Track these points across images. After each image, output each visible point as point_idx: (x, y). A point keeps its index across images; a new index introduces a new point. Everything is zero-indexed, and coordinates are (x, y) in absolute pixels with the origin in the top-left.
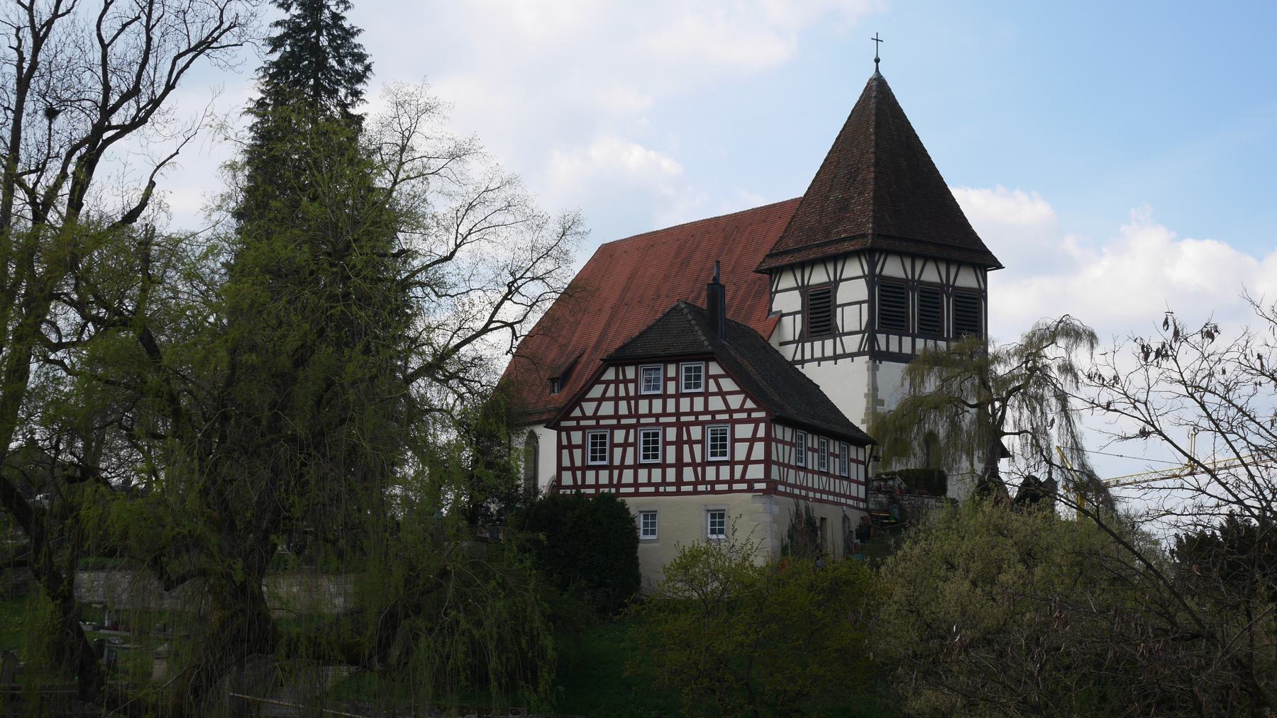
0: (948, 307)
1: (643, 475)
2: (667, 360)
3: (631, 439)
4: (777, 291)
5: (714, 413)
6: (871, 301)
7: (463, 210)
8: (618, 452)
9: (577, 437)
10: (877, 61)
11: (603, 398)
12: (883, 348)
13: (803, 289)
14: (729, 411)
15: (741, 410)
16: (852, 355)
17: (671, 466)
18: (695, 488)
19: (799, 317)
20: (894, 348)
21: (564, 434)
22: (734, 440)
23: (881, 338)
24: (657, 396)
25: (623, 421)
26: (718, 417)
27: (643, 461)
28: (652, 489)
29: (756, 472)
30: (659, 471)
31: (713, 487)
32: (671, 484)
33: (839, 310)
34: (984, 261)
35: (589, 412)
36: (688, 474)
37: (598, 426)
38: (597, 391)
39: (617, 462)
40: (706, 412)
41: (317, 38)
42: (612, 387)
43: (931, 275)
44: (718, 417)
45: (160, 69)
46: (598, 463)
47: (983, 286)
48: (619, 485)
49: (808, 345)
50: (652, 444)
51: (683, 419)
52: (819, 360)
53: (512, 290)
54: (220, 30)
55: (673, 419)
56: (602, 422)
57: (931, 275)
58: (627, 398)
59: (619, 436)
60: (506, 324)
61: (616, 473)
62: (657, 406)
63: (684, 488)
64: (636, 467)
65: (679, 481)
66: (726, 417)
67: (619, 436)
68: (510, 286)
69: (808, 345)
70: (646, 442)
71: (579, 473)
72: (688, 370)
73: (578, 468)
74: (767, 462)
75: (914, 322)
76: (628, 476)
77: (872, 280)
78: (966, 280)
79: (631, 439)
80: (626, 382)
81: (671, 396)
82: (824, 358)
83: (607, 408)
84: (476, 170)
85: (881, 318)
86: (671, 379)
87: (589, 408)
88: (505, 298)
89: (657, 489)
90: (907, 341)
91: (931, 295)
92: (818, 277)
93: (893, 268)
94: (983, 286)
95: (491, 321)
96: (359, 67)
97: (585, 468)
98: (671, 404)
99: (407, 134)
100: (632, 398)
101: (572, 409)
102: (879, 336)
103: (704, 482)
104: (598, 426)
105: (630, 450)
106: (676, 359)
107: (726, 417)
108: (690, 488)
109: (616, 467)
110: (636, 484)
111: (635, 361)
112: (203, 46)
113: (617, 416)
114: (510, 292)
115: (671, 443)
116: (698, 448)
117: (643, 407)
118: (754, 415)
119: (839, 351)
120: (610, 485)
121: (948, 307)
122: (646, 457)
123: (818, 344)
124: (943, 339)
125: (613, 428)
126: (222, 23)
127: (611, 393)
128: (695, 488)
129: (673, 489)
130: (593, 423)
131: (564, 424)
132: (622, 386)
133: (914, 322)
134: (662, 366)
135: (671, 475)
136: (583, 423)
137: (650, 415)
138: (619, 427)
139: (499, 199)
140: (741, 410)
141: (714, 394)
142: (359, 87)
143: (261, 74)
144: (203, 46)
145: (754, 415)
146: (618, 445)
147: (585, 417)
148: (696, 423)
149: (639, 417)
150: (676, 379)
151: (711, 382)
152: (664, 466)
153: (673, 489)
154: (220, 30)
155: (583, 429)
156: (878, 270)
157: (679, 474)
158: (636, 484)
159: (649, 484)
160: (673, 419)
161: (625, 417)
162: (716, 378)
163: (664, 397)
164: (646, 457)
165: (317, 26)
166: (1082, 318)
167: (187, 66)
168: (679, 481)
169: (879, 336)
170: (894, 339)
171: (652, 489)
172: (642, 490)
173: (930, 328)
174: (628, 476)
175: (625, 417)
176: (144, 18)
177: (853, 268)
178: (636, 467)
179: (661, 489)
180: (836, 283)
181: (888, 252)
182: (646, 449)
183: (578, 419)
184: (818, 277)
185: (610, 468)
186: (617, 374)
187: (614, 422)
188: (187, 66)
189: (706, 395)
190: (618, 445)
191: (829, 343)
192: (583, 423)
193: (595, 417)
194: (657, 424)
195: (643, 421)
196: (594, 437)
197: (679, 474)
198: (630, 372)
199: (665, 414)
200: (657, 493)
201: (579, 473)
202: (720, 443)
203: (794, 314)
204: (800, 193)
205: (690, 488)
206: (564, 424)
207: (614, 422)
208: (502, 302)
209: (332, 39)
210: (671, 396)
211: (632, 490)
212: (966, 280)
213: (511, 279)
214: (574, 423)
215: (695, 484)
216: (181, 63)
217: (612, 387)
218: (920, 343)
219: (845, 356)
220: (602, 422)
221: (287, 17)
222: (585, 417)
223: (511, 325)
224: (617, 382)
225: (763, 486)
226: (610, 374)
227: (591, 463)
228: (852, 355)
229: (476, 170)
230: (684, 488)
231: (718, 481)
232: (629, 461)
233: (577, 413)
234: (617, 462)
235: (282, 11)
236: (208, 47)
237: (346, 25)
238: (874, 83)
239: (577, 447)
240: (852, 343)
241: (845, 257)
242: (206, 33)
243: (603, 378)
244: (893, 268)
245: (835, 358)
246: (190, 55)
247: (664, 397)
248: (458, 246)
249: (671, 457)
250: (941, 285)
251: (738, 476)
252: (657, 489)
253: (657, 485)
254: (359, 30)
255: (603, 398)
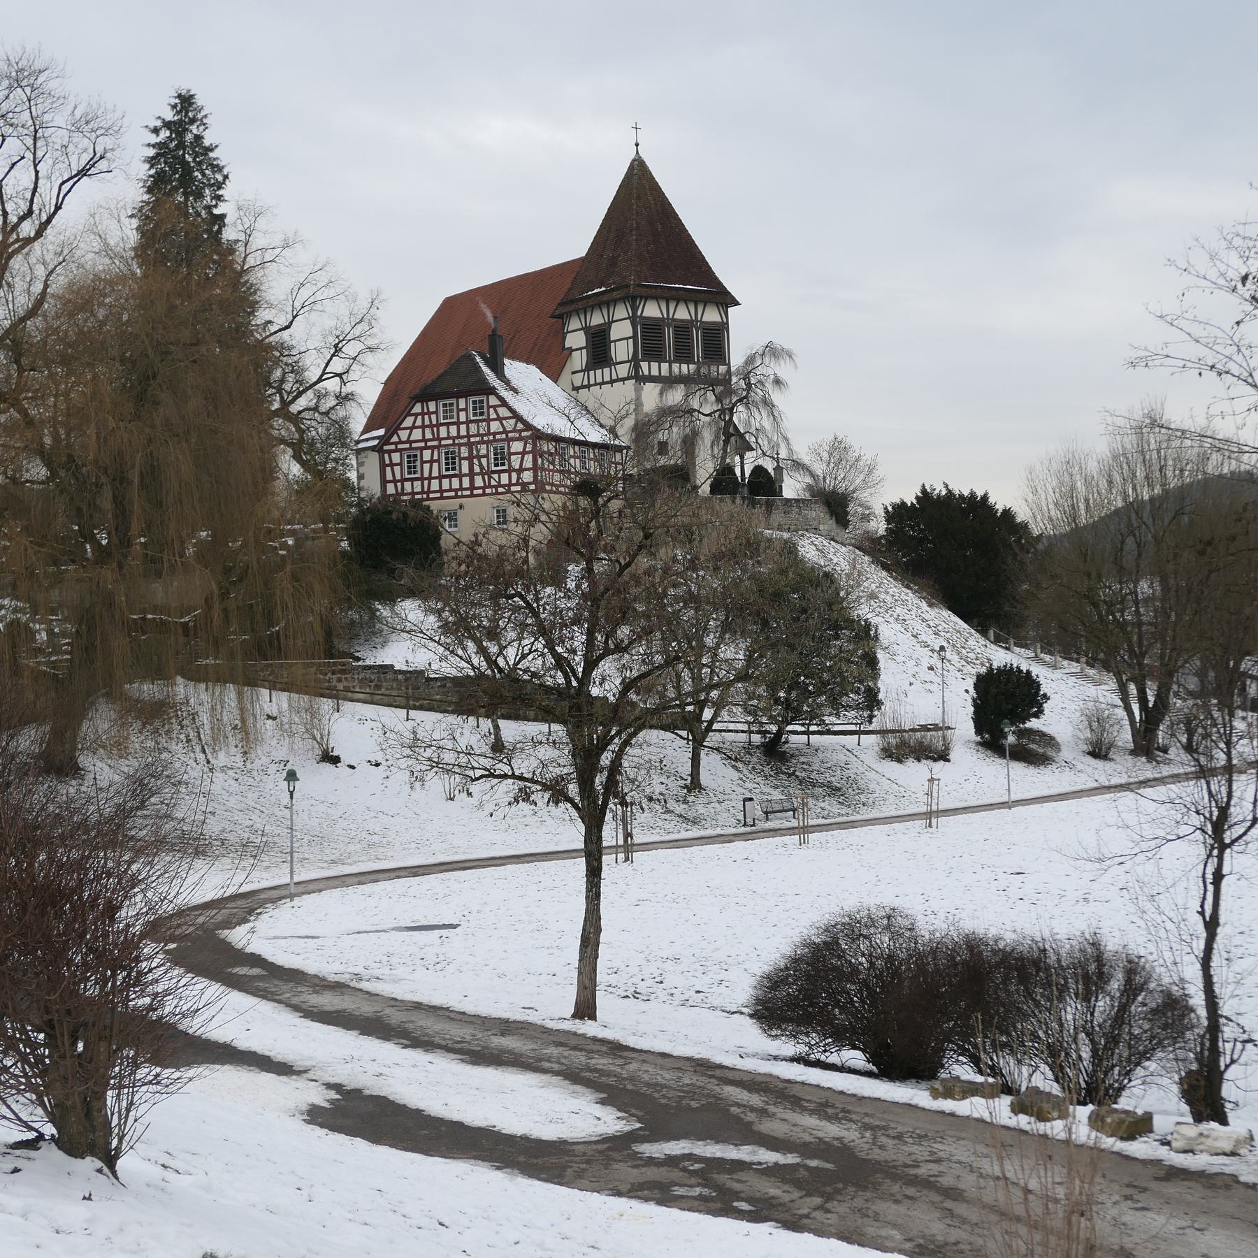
0: (697, 338)
1: (445, 482)
2: (458, 396)
3: (436, 457)
4: (568, 332)
5: (495, 434)
6: (634, 337)
7: (296, 288)
8: (426, 466)
9: (396, 457)
10: (637, 145)
11: (413, 427)
12: (646, 373)
13: (586, 329)
14: (505, 432)
15: (514, 431)
16: (623, 380)
17: (465, 475)
18: (484, 491)
19: (584, 351)
20: (655, 372)
21: (386, 456)
22: (510, 454)
23: (644, 365)
24: (453, 424)
25: (429, 444)
26: (498, 437)
27: (445, 473)
28: (453, 494)
29: (527, 476)
30: (419, 483)
31: (497, 490)
32: (466, 489)
33: (612, 344)
34: (724, 299)
35: (404, 438)
36: (479, 481)
37: (411, 448)
38: (408, 422)
39: (426, 475)
40: (489, 433)
41: (183, 155)
42: (420, 418)
43: (682, 313)
44: (498, 437)
45: (48, 193)
46: (413, 476)
47: (725, 320)
48: (429, 492)
49: (592, 373)
50: (452, 460)
51: (472, 440)
52: (600, 384)
53: (337, 350)
54: (92, 163)
55: (465, 440)
56: (414, 445)
57: (682, 313)
58: (431, 426)
59: (427, 455)
60: (337, 375)
61: (426, 482)
62: (453, 429)
63: (476, 492)
64: (441, 477)
65: (472, 487)
66: (504, 436)
67: (427, 455)
68: (336, 346)
69: (592, 373)
70: (447, 459)
71: (399, 485)
72: (474, 402)
73: (398, 481)
74: (535, 468)
75: (670, 351)
76: (435, 485)
77: (633, 319)
78: (711, 315)
79: (436, 457)
80: (429, 413)
81: (463, 423)
82: (604, 383)
83: (417, 435)
84: (301, 258)
85: (643, 350)
86: (462, 410)
87: (404, 435)
88: (333, 355)
89: (456, 494)
90: (665, 366)
91: (683, 330)
92: (597, 319)
93: (652, 310)
94: (725, 320)
95: (324, 373)
96: (220, 178)
97: (403, 480)
98: (463, 427)
99: (248, 232)
100: (435, 426)
101: (391, 436)
102: (642, 364)
103: (490, 486)
104: (411, 448)
105: (435, 465)
106: (465, 395)
107: (504, 436)
108: (480, 492)
109: (426, 479)
110: (441, 491)
111: (436, 397)
112: (83, 173)
113: (424, 440)
114: (336, 351)
115: (465, 458)
116: (397, 469)
117: (443, 432)
118: (523, 434)
119: (614, 377)
120: (422, 492)
121: (697, 338)
122: (447, 469)
123: (599, 372)
124: (694, 363)
125: (422, 449)
126: (95, 154)
127: (419, 423)
128: (484, 491)
129: (468, 493)
130: (407, 446)
131: (386, 448)
132: (426, 417)
133: (670, 351)
134: (454, 401)
135: (466, 482)
136: (400, 446)
137: (448, 438)
138: (426, 448)
139: (322, 278)
140: (514, 431)
141: (494, 420)
142: (220, 192)
143: (141, 184)
144: (83, 173)
145: (523, 434)
146: (426, 462)
147: (401, 442)
148: (483, 442)
149: (440, 439)
150: (466, 410)
151: (492, 410)
152: (460, 476)
153: (468, 493)
154: (92, 163)
155: (400, 451)
156: (639, 313)
157: (472, 481)
158: (441, 491)
159: (451, 490)
160: (465, 440)
161: (430, 440)
162: (495, 407)
163: (458, 424)
164: (447, 469)
165: (182, 145)
166: (780, 341)
167: (69, 191)
168: (472, 487)
169: (642, 364)
170: (655, 365)
171: (453, 494)
172: (445, 494)
173: (684, 354)
174: (435, 485)
175: (430, 440)
176: (29, 155)
177: (621, 311)
178: (441, 477)
179: (459, 493)
180: (610, 323)
181: (646, 298)
182: (447, 464)
183: (396, 444)
184: (597, 319)
185: (422, 479)
186: (423, 409)
187: (423, 444)
188: (69, 191)
189: (488, 420)
190: (426, 462)
191: (607, 370)
192: (400, 446)
193: (408, 441)
194: (454, 444)
195: (443, 442)
196: (409, 457)
197: (472, 481)
198: (432, 406)
199: (459, 437)
200: (456, 497)
201: (399, 485)
202: (502, 457)
203: (581, 349)
204: (583, 254)
205: (480, 492)
206: (386, 448)
207: (423, 444)
208: (331, 359)
209: (196, 155)
210: (463, 423)
211: (438, 495)
212: (711, 315)
213: (337, 341)
214: (393, 447)
215: (483, 488)
216: (66, 188)
217: (420, 418)
218: (675, 367)
219: (618, 380)
220: (414, 445)
221: (158, 140)
222: (401, 442)
223: (340, 375)
224: (423, 414)
225: (532, 487)
226: (417, 408)
227: (407, 476)
228: (623, 380)
229: (301, 258)
230: (476, 492)
231: (461, 489)
232: (435, 473)
233: (395, 439)
234: (426, 475)
235: (154, 135)
236: (85, 175)
237: (207, 143)
238: (636, 163)
239: (397, 464)
240: (623, 370)
241: (615, 301)
242: (83, 163)
243: (412, 412)
244: (652, 310)
245: (612, 382)
246: (71, 182)
247: (458, 424)
248: (294, 317)
249: (465, 469)
250: (691, 321)
251: (514, 480)
252: (456, 494)
253: (456, 491)
254: (216, 146)
255: (413, 427)
